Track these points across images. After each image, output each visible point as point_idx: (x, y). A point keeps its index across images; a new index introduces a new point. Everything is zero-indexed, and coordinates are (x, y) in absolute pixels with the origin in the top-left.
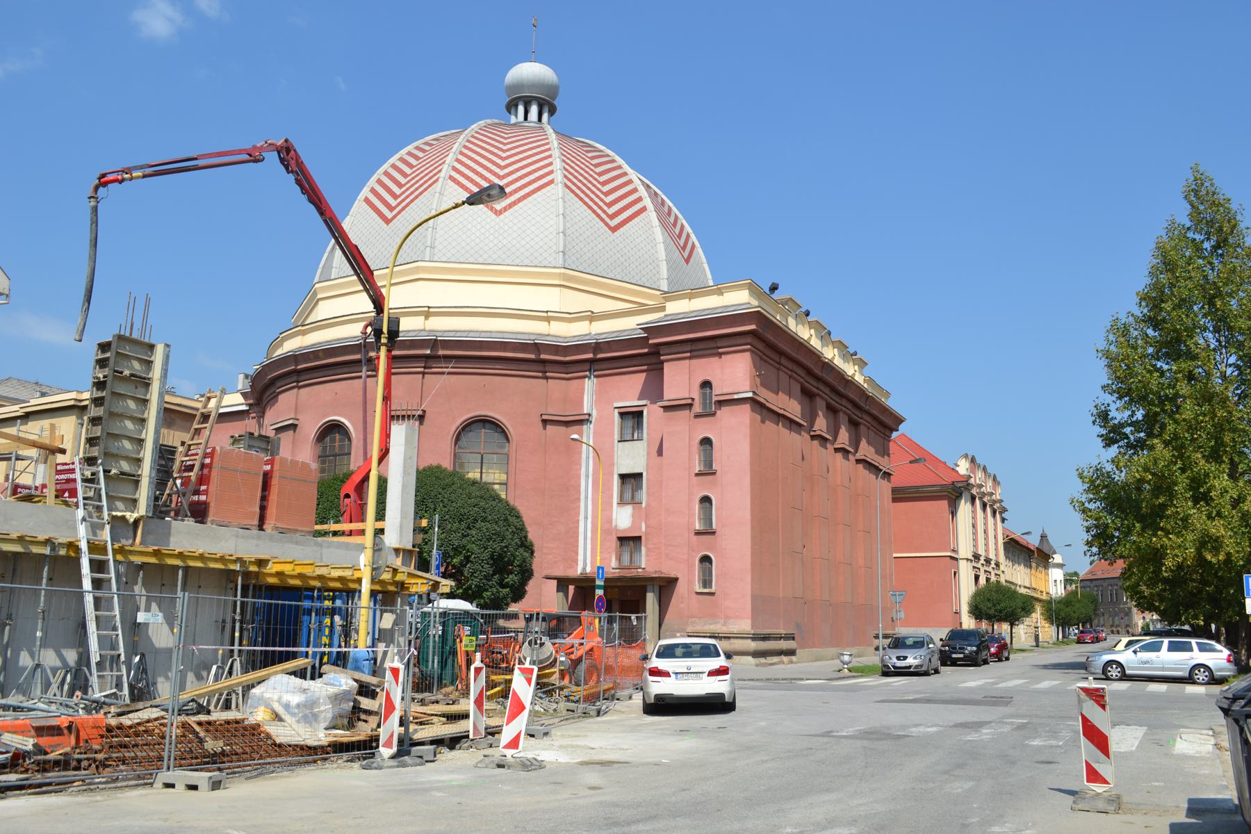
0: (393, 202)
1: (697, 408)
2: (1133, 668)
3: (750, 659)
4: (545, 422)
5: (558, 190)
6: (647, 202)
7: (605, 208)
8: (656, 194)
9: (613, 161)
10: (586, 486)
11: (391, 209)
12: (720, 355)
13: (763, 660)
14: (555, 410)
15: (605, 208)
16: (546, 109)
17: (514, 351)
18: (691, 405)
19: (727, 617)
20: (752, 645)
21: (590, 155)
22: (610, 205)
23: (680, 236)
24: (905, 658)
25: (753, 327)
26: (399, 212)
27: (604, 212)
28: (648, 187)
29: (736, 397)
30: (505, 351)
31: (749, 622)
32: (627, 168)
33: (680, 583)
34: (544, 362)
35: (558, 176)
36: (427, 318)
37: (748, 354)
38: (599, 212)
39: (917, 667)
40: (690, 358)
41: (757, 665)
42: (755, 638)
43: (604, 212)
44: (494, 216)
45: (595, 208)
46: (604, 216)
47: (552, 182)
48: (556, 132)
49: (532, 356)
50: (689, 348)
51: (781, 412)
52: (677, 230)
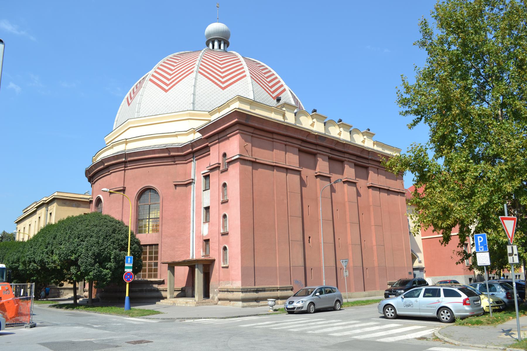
1: (221, 169)
2: (400, 310)
3: (240, 303)
4: (176, 185)
5: (248, 79)
9: (267, 68)
10: (192, 215)
11: (167, 85)
12: (228, 138)
13: (245, 304)
14: (181, 179)
17: (159, 153)
18: (219, 167)
19: (233, 280)
20: (241, 295)
22: (271, 87)
24: (293, 302)
25: (236, 120)
26: (172, 87)
27: (269, 90)
29: (233, 159)
30: (155, 154)
31: (240, 282)
32: (273, 72)
33: (216, 261)
34: (174, 156)
35: (247, 73)
36: (126, 144)
37: (238, 135)
39: (299, 308)
40: (219, 142)
41: (243, 307)
42: (243, 291)
43: (269, 90)
49: (167, 155)
50: (217, 138)
51: (274, 164)
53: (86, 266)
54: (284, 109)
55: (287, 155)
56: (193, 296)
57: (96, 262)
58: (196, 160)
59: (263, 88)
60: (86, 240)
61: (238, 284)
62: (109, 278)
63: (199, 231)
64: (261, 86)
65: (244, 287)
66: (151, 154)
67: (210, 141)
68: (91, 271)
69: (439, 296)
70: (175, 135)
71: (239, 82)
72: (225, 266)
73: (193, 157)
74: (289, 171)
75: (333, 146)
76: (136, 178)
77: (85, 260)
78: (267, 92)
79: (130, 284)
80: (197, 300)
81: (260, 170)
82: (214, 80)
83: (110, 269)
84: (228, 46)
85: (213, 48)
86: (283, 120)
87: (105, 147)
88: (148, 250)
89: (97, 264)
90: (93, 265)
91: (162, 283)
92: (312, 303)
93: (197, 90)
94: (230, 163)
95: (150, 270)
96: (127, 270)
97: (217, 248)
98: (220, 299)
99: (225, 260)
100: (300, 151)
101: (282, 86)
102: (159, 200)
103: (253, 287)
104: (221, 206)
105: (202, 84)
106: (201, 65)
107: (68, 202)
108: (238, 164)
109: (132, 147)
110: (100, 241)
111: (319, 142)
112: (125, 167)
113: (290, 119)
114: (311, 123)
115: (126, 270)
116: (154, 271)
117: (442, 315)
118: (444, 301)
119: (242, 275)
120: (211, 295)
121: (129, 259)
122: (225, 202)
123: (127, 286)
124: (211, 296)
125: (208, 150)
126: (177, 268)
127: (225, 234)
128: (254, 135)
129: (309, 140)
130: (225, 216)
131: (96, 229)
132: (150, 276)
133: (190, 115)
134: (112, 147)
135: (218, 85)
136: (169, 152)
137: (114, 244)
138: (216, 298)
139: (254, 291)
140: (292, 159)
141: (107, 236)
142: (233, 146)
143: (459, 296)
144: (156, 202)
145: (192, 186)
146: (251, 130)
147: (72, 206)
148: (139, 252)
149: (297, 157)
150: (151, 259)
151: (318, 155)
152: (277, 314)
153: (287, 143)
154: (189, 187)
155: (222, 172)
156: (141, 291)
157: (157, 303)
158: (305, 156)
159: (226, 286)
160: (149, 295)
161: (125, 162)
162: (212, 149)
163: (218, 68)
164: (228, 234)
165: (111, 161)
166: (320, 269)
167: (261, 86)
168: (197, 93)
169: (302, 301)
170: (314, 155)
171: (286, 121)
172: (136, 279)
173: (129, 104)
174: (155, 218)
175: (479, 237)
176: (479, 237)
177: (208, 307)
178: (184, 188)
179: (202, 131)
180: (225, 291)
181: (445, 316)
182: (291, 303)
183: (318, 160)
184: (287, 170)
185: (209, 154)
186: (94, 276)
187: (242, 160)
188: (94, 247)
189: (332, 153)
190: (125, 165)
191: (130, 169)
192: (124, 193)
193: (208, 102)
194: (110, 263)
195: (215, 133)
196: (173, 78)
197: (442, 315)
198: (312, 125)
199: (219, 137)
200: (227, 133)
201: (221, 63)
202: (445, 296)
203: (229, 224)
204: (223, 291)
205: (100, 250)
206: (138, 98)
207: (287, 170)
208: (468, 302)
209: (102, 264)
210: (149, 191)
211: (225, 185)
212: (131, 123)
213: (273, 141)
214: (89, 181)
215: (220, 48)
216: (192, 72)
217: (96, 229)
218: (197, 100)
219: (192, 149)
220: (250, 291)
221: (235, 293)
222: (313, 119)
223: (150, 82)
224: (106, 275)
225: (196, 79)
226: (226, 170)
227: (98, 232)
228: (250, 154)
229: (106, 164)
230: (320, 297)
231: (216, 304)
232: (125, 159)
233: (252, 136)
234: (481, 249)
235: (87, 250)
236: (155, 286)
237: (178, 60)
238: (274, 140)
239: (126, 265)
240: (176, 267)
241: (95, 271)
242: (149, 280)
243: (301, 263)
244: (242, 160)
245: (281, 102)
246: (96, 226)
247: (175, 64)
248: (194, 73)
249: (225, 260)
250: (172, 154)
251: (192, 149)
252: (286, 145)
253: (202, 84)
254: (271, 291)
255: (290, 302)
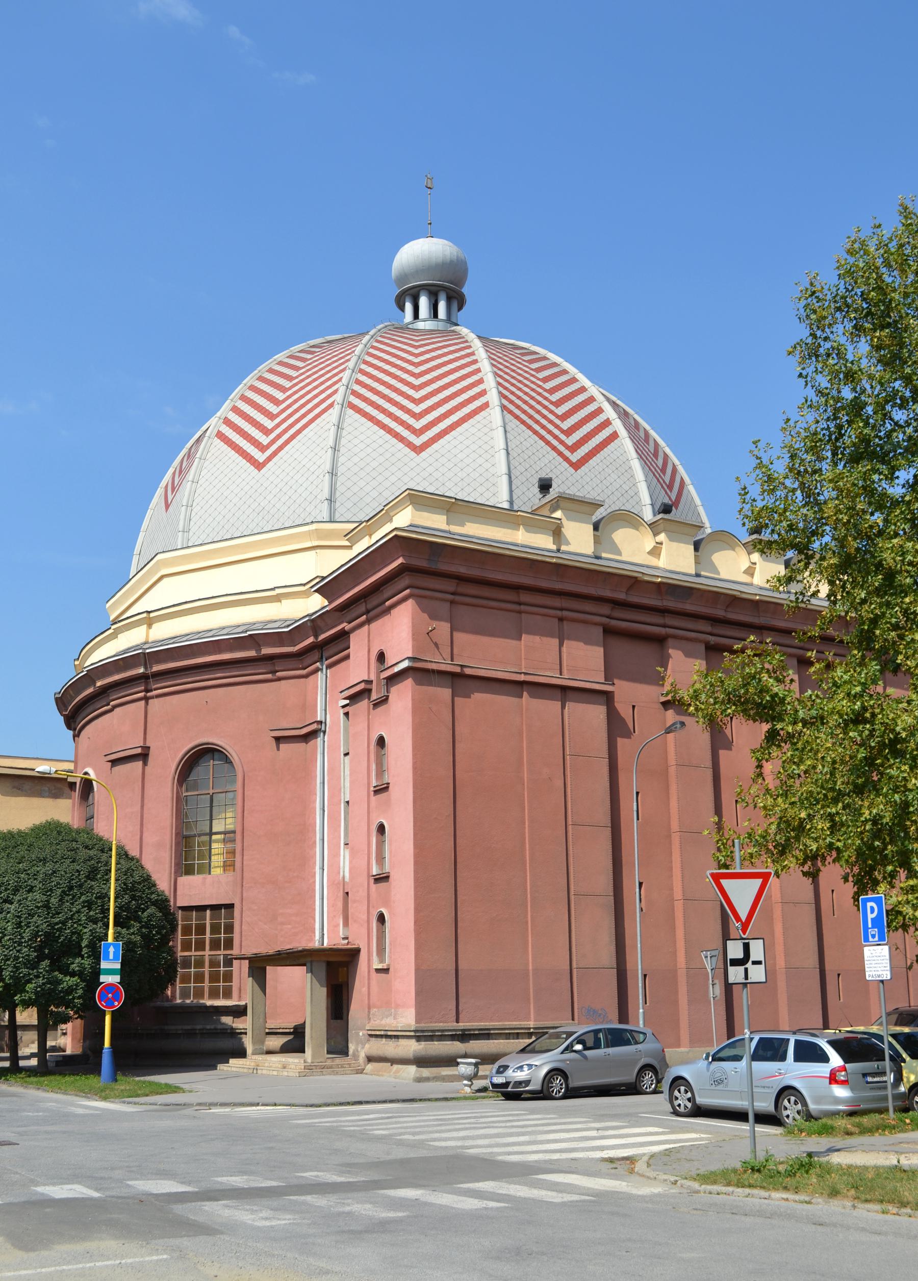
0: (264, 440)
1: (374, 696)
3: (412, 1070)
4: (278, 739)
5: (495, 414)
6: (617, 425)
7: (563, 437)
8: (626, 414)
9: (565, 372)
11: (262, 448)
13: (426, 1072)
14: (292, 722)
15: (563, 437)
16: (455, 306)
18: (369, 691)
19: (397, 1006)
20: (412, 1047)
21: (535, 366)
22: (568, 432)
23: (663, 470)
24: (506, 1067)
25: (400, 561)
26: (275, 454)
27: (562, 442)
28: (614, 405)
32: (584, 381)
34: (271, 658)
35: (493, 396)
36: (150, 626)
37: (410, 603)
38: (555, 442)
39: (519, 1083)
40: (368, 621)
41: (419, 1080)
42: (421, 1036)
44: (413, 454)
45: (549, 437)
46: (561, 448)
47: (486, 405)
48: (479, 337)
49: (252, 653)
50: (362, 608)
51: (522, 678)
52: (660, 462)
53: (17, 968)
54: (558, 514)
55: (564, 649)
56: (302, 1050)
57: (40, 958)
58: (329, 667)
59: (542, 438)
60: (17, 898)
61: (407, 1018)
62: (79, 998)
63: (335, 867)
64: (536, 432)
65: (423, 1026)
66: (210, 654)
67: (349, 618)
68: (29, 981)
69: (783, 1058)
70: (275, 596)
71: (465, 425)
72: (380, 966)
73: (321, 660)
74: (570, 694)
75: (720, 613)
76: (176, 721)
77: (14, 953)
78: (554, 448)
79: (113, 1014)
80: (309, 1060)
81: (478, 696)
82: (549, 437)
83: (80, 974)
84: (460, 308)
85: (416, 315)
86: (554, 547)
87: (121, 624)
88: (208, 922)
89: (45, 963)
90: (34, 965)
91: (240, 1012)
92: (555, 1072)
93: (342, 460)
94: (393, 679)
95: (214, 977)
96: (105, 979)
97: (365, 917)
98: (370, 1059)
99: (381, 951)
100: (608, 632)
101: (607, 423)
102: (234, 781)
103: (453, 1025)
104: (373, 798)
105: (356, 441)
106: (358, 382)
107: (27, 785)
108: (408, 684)
109: (165, 632)
110: (54, 901)
111: (670, 603)
112: (147, 691)
113: (579, 541)
114: (648, 549)
115: (103, 978)
116: (222, 981)
117: (786, 1109)
118: (792, 1071)
119: (418, 993)
120: (352, 1047)
121: (112, 950)
122: (382, 790)
123: (108, 1019)
124: (351, 1052)
125: (342, 646)
126: (272, 972)
127: (382, 879)
128: (457, 598)
129: (634, 599)
130: (381, 829)
131: (42, 869)
132: (214, 994)
133: (319, 534)
134: (114, 636)
135: (401, 439)
136: (258, 647)
137: (90, 909)
138: (362, 1055)
139: (453, 1038)
140: (584, 660)
141: (71, 888)
142: (398, 633)
143: (824, 1058)
144: (229, 788)
145: (319, 740)
146: (450, 586)
147: (40, 795)
148: (163, 927)
149: (598, 652)
150: (215, 945)
151: (670, 641)
152: (484, 1098)
153: (565, 613)
154: (312, 743)
155: (376, 705)
156: (191, 1034)
157: (221, 1067)
158: (623, 648)
159: (383, 1022)
160: (210, 1044)
161: (144, 678)
162: (353, 637)
163: (405, 389)
164: (388, 877)
165: (110, 674)
166: (674, 972)
167: (536, 432)
168: (341, 470)
169: (530, 1066)
170: (660, 641)
171: (563, 548)
172: (179, 1001)
173: (167, 506)
174: (225, 833)
175: (869, 904)
176: (869, 904)
177: (340, 1081)
178: (300, 746)
179: (327, 588)
180: (381, 1036)
181: (790, 1110)
182: (503, 1069)
183: (669, 656)
184: (565, 692)
185: (347, 657)
186: (36, 993)
187: (418, 672)
188: (35, 919)
189: (716, 631)
190: (147, 684)
191: (158, 696)
192: (145, 764)
193: (374, 494)
194: (78, 960)
195: (356, 596)
196: (278, 426)
197: (786, 1109)
198: (655, 551)
199: (370, 606)
200: (386, 596)
201: (417, 371)
202: (795, 1061)
203: (391, 852)
204: (377, 1036)
205: (52, 925)
206: (186, 488)
207: (565, 692)
208: (841, 1076)
209: (59, 965)
210: (209, 756)
211: (381, 742)
212: (165, 563)
213: (520, 612)
214: (69, 726)
215: (435, 315)
216: (331, 405)
217: (42, 869)
218: (340, 489)
219: (316, 637)
220: (442, 1038)
221: (403, 1042)
222: (655, 534)
223: (217, 441)
224: (70, 990)
225: (339, 427)
226: (384, 700)
227: (49, 876)
228: (446, 652)
229: (99, 684)
230: (585, 1057)
231: (361, 1071)
232: (146, 668)
233: (452, 602)
234: (873, 936)
235: (19, 925)
236: (227, 1020)
237: (297, 368)
238: (523, 607)
239: (104, 965)
240: (270, 970)
241: (41, 981)
242: (209, 1003)
243: (607, 956)
244: (418, 672)
245: (553, 493)
246: (44, 860)
247: (287, 384)
248: (337, 408)
249: (381, 951)
250: (266, 651)
251: (316, 637)
252: (561, 619)
253: (356, 441)
254: (508, 1036)
255: (500, 1067)
